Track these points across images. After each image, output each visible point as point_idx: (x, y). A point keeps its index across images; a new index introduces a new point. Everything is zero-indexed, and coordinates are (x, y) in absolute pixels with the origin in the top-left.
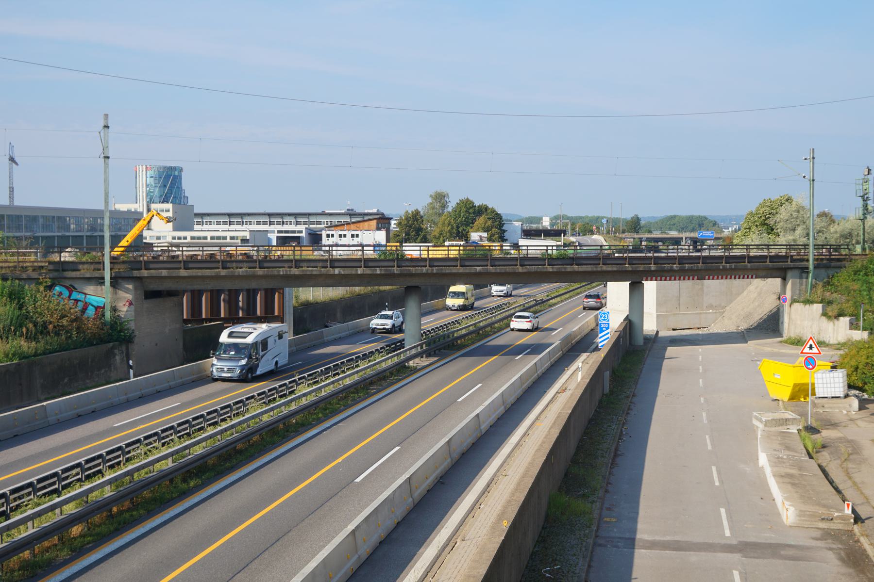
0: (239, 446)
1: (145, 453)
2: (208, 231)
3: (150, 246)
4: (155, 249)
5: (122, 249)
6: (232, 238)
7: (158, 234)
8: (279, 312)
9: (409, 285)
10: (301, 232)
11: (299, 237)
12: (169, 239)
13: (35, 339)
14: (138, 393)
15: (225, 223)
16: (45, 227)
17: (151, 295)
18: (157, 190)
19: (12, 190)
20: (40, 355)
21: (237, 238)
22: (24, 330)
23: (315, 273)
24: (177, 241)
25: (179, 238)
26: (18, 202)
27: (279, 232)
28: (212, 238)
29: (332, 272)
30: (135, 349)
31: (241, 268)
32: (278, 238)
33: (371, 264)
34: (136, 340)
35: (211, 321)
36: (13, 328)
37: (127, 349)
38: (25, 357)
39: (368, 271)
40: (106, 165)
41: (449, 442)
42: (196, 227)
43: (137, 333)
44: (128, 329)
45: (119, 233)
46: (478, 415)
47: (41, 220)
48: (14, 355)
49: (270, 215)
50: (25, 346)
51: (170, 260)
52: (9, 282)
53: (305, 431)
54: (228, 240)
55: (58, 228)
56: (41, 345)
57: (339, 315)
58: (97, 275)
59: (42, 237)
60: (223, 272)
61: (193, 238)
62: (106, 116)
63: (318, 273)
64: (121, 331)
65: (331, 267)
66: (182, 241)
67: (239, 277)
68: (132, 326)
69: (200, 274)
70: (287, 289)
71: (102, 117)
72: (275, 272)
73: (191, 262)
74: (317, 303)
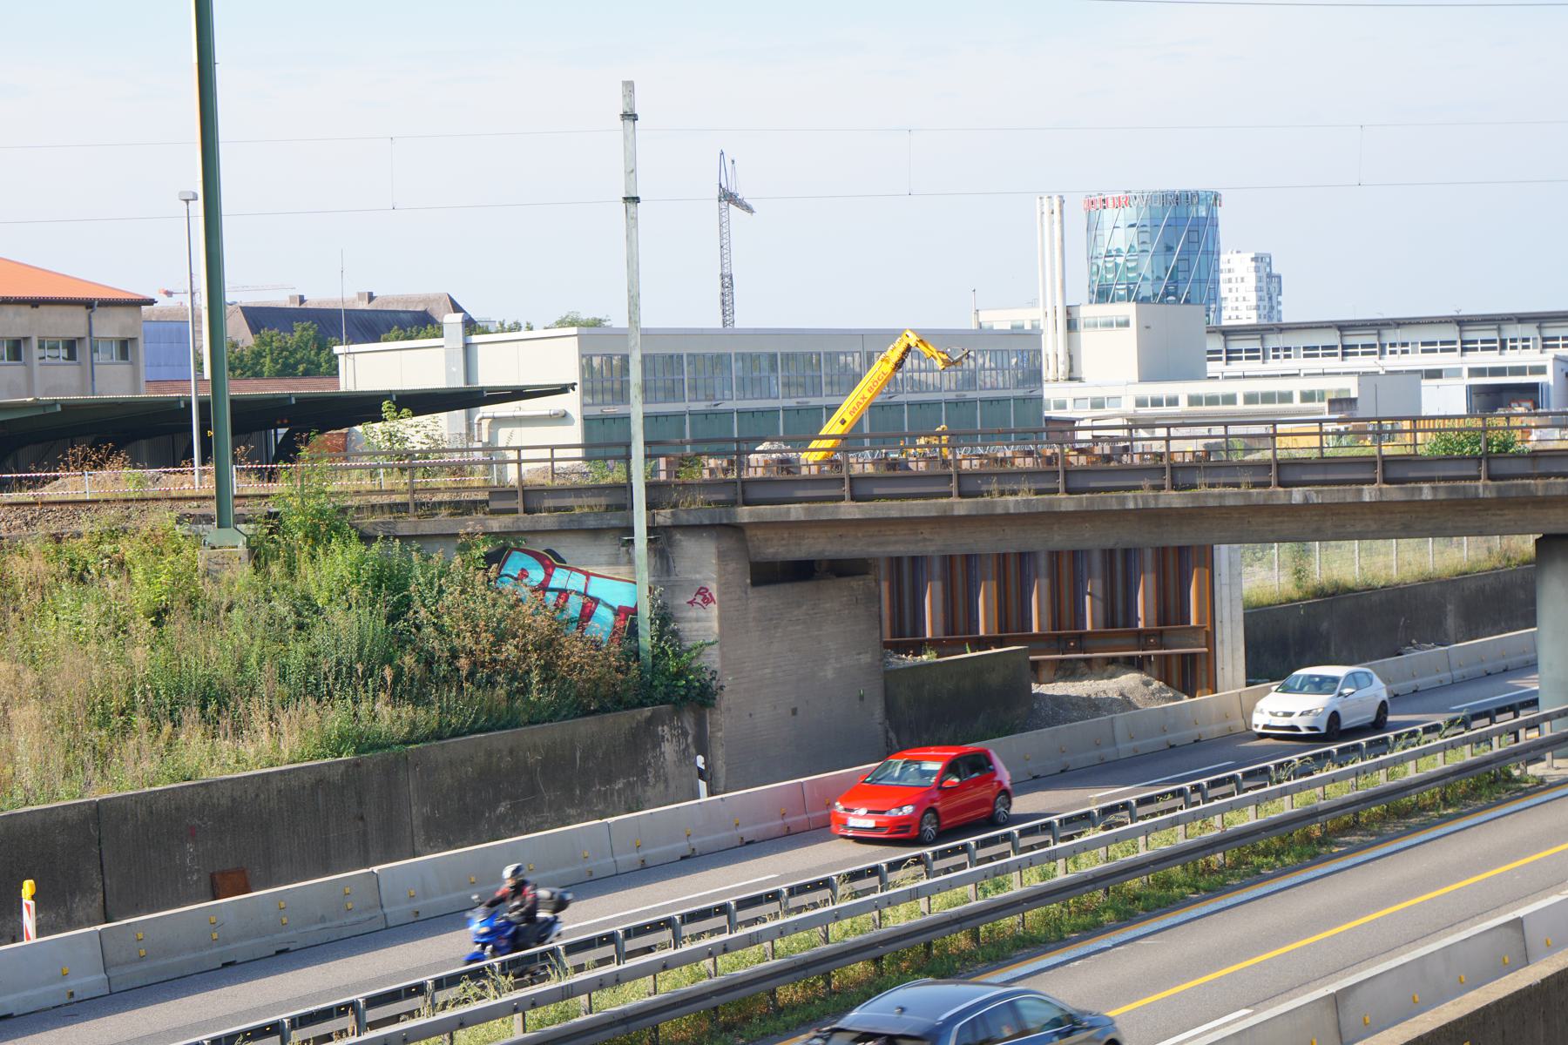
0: (787, 993)
5: (829, 444)
6: (1307, 397)
7: (1098, 393)
9: (1552, 529)
10: (1541, 370)
11: (1534, 388)
12: (1128, 407)
14: (682, 847)
15: (1329, 350)
16: (748, 385)
17: (766, 574)
18: (1146, 261)
19: (727, 282)
20: (426, 739)
21: (1322, 396)
22: (388, 673)
23: (1230, 502)
25: (1157, 402)
26: (747, 317)
27: (1476, 372)
28: (1250, 399)
29: (1283, 500)
30: (723, 723)
31: (1014, 493)
34: (725, 700)
35: (1000, 642)
37: (700, 724)
39: (1394, 493)
41: (1336, 1000)
43: (728, 680)
45: (814, 401)
46: (1518, 924)
47: (736, 367)
48: (343, 738)
49: (1462, 322)
50: (387, 716)
51: (882, 471)
52: (376, 546)
54: (1297, 403)
56: (427, 718)
57: (1451, 622)
58: (615, 522)
59: (910, 404)
60: (962, 506)
61: (1194, 400)
62: (629, 86)
63: (1240, 502)
64: (680, 674)
65: (1280, 484)
67: (1009, 518)
68: (712, 659)
69: (895, 514)
70: (1224, 547)
71: (619, 90)
72: (1111, 501)
73: (1179, 474)
74: (1370, 589)
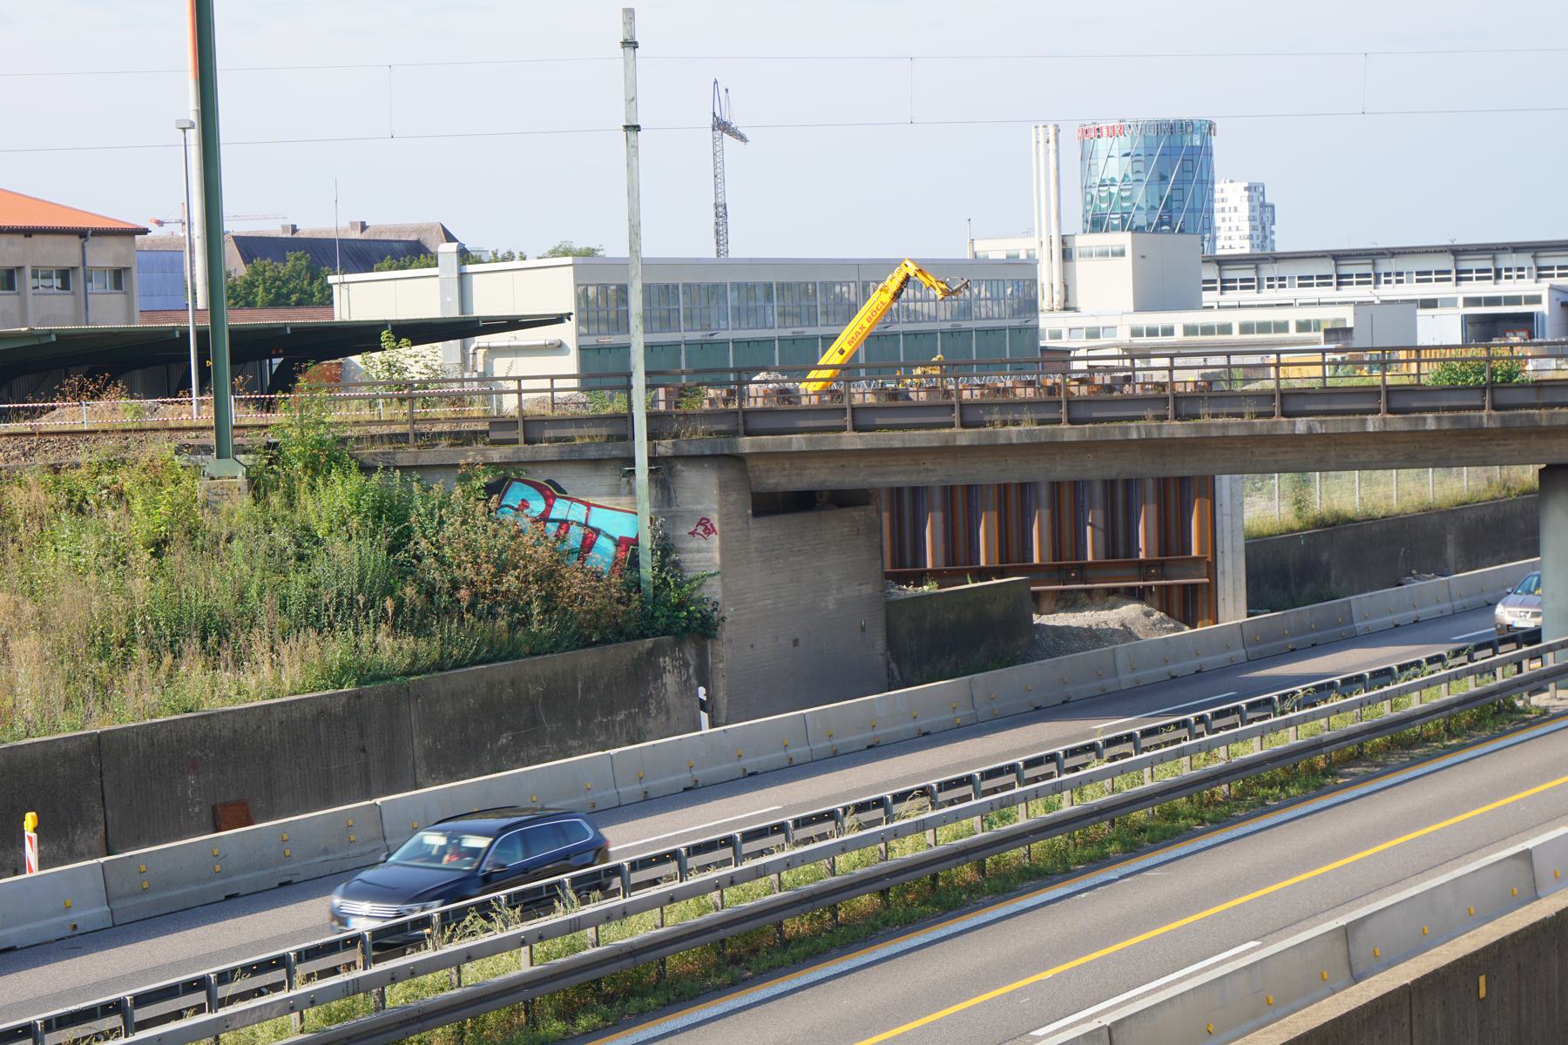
1: (755, 951)
2: (1230, 311)
3: (1063, 355)
4: (1076, 365)
5: (827, 374)
6: (1303, 326)
7: (1093, 323)
8: (1201, 550)
9: (1555, 459)
10: (1536, 300)
11: (1528, 318)
12: (1124, 336)
13: (420, 630)
15: (1324, 280)
16: (743, 315)
17: (768, 505)
19: (721, 211)
20: (428, 670)
22: (389, 604)
23: (1233, 432)
24: (1145, 340)
25: (1152, 332)
26: (742, 247)
27: (1470, 302)
28: (1246, 328)
30: (725, 654)
31: (1016, 423)
32: (1468, 321)
33: (1399, 402)
34: (726, 632)
35: (1001, 573)
36: (361, 599)
37: (702, 655)
38: (377, 678)
39: (1398, 423)
40: (632, 149)
41: (1347, 932)
42: (1209, 297)
44: (701, 600)
46: (1526, 855)
47: (731, 297)
48: (344, 669)
50: (388, 648)
51: (884, 402)
52: (376, 477)
53: (1035, 889)
54: (1292, 333)
55: (783, 315)
56: (428, 649)
57: (1451, 552)
59: (1011, 329)
61: (1190, 330)
62: (629, 13)
63: (1243, 432)
64: (681, 606)
65: (1284, 414)
66: (1160, 339)
67: (1011, 448)
68: (713, 591)
69: (897, 444)
70: (1226, 478)
71: (619, 18)
72: (1114, 431)
